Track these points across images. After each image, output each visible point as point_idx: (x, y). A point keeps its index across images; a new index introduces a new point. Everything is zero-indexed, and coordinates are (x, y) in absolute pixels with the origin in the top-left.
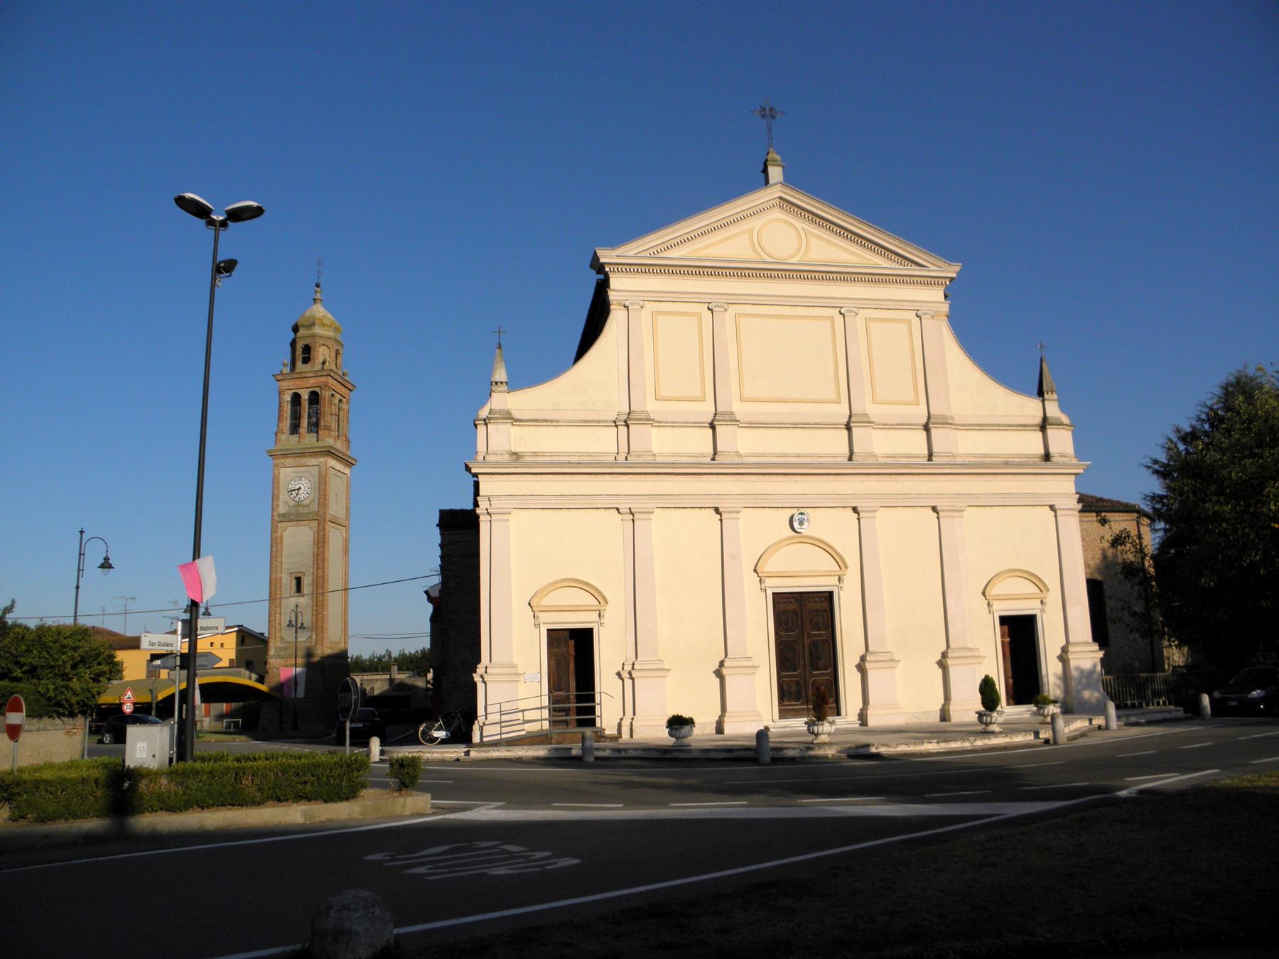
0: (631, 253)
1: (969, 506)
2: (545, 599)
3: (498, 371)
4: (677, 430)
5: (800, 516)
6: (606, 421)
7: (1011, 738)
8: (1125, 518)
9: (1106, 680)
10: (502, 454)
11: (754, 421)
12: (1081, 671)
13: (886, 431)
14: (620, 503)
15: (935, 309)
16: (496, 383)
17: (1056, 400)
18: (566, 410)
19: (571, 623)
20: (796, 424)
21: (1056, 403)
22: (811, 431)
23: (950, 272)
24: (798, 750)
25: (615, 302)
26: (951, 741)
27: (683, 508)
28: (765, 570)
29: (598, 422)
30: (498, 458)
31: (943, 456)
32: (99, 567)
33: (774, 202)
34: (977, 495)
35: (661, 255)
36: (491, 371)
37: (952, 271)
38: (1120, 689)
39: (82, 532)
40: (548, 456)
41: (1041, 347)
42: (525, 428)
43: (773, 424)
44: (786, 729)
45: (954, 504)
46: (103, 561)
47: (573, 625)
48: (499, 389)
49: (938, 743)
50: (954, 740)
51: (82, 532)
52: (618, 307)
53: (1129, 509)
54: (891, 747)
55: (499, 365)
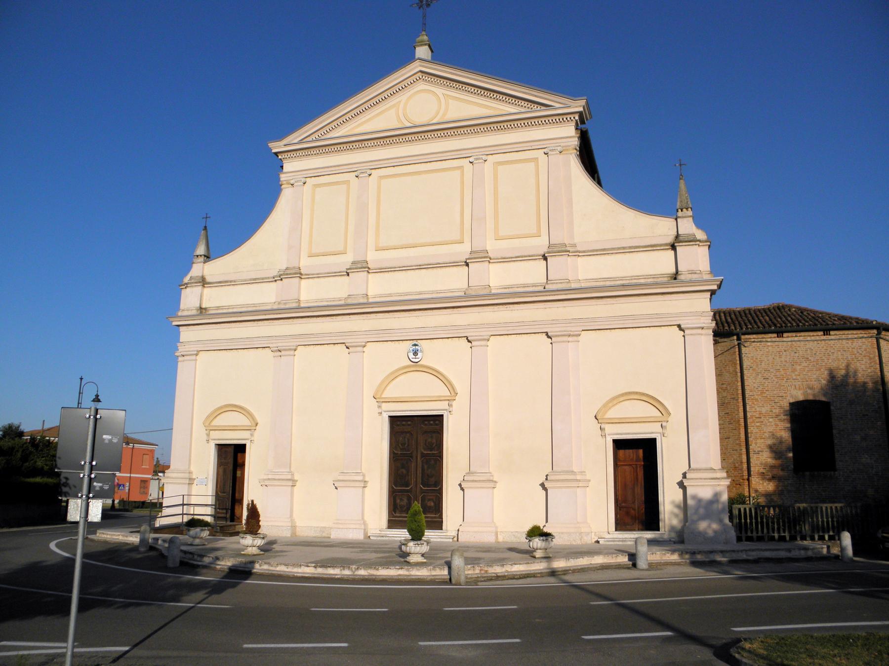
0: (296, 141)
1: (583, 330)
2: (216, 420)
3: (200, 247)
4: (322, 280)
5: (414, 347)
6: (269, 278)
7: (408, 570)
8: (861, 335)
9: (831, 508)
10: (192, 310)
11: (384, 266)
12: (699, 501)
13: (505, 264)
14: (272, 343)
15: (562, 144)
16: (197, 256)
17: (690, 216)
18: (243, 272)
19: (231, 440)
20: (420, 266)
21: (691, 219)
22: (435, 270)
23: (576, 107)
24: (211, 559)
25: (285, 182)
26: (329, 567)
27: (320, 344)
28: (383, 396)
29: (263, 279)
30: (189, 313)
31: (557, 283)
32: (92, 401)
33: (417, 76)
34: (593, 320)
35: (329, 136)
36: (195, 246)
37: (578, 106)
38: (825, 520)
39: (81, 379)
40: (225, 309)
41: (680, 165)
42: (214, 289)
43: (400, 267)
44: (384, 538)
45: (569, 329)
46: (95, 397)
47: (232, 441)
48: (198, 261)
49: (315, 567)
50: (333, 567)
51: (81, 379)
52: (287, 186)
53: (865, 325)
54: (272, 566)
55: (201, 243)
